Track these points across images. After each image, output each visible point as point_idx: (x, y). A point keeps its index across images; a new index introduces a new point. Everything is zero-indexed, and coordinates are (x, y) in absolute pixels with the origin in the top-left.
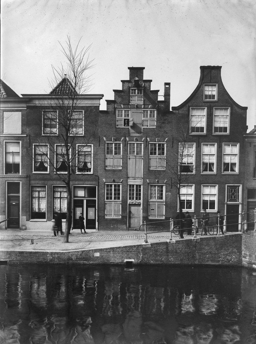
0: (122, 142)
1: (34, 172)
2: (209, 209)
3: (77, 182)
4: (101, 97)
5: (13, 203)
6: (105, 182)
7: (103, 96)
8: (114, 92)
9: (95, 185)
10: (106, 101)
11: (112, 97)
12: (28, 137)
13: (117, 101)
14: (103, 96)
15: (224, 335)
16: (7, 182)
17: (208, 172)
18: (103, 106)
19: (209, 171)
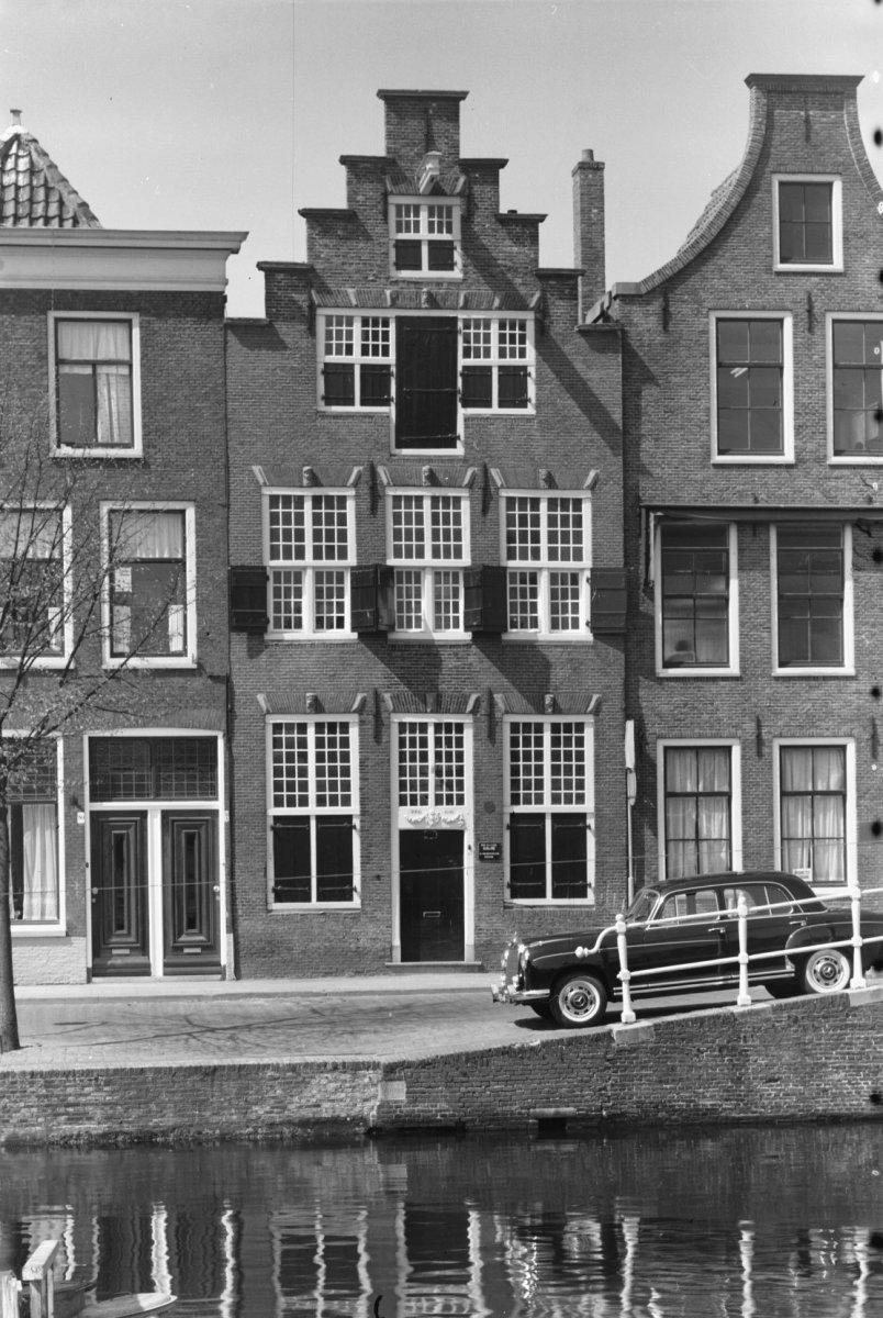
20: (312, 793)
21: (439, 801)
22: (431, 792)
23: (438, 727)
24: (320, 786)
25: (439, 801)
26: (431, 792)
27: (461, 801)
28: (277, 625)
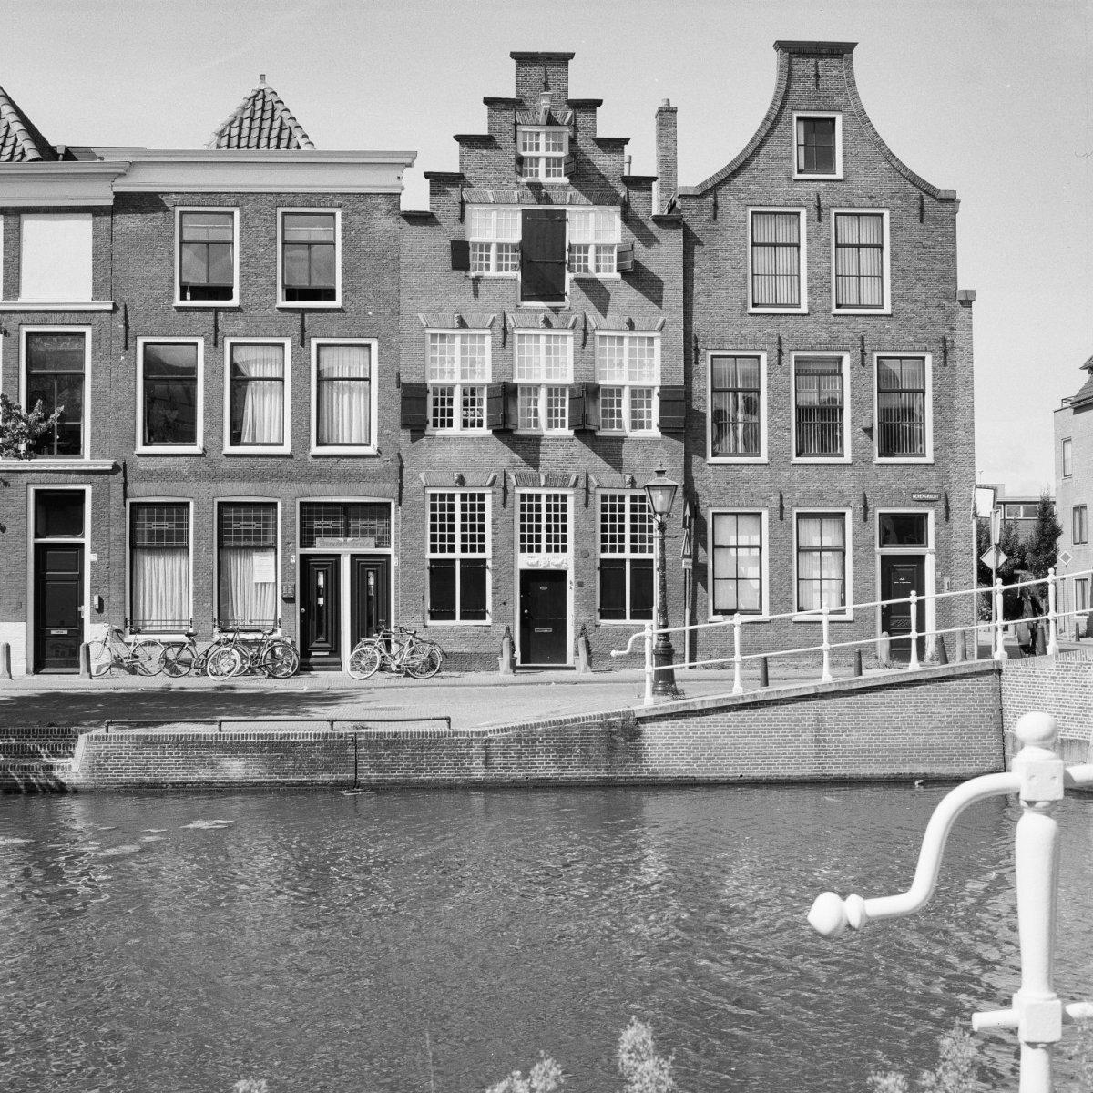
0: (489, 332)
1: (141, 449)
2: (631, 618)
3: (317, 487)
4: (408, 160)
5: (327, 654)
6: (427, 486)
7: (414, 155)
8: (458, 143)
9: (384, 496)
10: (427, 175)
11: (449, 160)
12: (120, 313)
13: (467, 175)
14: (414, 155)
15: (229, 553)
16: (37, 492)
17: (458, 622)
18: (417, 197)
19: (462, 618)
20: (458, 543)
21: (549, 549)
22: (543, 543)
23: (548, 497)
24: (464, 538)
25: (549, 549)
26: (543, 543)
27: (564, 549)
28: (435, 425)
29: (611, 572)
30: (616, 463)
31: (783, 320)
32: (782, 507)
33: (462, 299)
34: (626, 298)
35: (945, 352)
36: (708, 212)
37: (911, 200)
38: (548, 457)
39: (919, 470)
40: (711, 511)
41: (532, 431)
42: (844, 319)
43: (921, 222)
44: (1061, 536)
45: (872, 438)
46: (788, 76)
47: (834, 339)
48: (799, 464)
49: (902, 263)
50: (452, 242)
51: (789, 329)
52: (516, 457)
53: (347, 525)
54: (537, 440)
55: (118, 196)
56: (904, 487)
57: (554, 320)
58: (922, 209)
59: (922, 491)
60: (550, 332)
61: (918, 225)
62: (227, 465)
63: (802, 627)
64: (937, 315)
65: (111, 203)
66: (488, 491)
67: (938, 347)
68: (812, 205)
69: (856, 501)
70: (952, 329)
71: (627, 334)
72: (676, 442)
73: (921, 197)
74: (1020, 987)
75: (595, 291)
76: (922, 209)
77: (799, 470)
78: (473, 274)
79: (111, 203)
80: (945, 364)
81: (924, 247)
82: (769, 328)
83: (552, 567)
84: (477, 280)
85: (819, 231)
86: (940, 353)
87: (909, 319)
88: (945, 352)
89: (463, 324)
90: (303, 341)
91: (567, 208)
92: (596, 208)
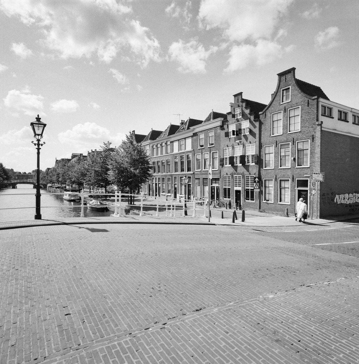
0: (255, 144)
1: (196, 170)
29: (247, 191)
30: (248, 171)
31: (277, 137)
32: (276, 178)
33: (227, 142)
34: (250, 138)
35: (313, 138)
36: (264, 116)
37: (306, 102)
38: (239, 169)
39: (305, 169)
40: (264, 179)
41: (236, 165)
42: (290, 134)
43: (308, 106)
44: (3, 164)
45: (295, 162)
46: (280, 81)
47: (287, 139)
48: (298, 168)
49: (303, 118)
50: (225, 132)
51: (278, 139)
52: (234, 170)
53: (216, 182)
54: (237, 166)
55: (193, 134)
56: (302, 173)
57: (240, 144)
58: (308, 103)
59: (306, 174)
60: (239, 146)
61: (307, 107)
62: (203, 172)
63: (280, 205)
64: (311, 129)
65: (192, 135)
66: (230, 176)
67: (311, 138)
68: (284, 109)
69: (291, 177)
70: (315, 132)
71: (250, 144)
72: (257, 165)
73: (308, 100)
74: (63, 159)
75: (245, 136)
76: (308, 103)
77: (280, 170)
78: (229, 137)
79: (192, 135)
80: (313, 142)
81: (309, 113)
82: (275, 139)
83: (239, 190)
84: (230, 138)
85: (285, 114)
86: (312, 139)
87: (304, 132)
88: (313, 138)
89: (228, 147)
90: (202, 154)
91: (241, 122)
92: (245, 121)
